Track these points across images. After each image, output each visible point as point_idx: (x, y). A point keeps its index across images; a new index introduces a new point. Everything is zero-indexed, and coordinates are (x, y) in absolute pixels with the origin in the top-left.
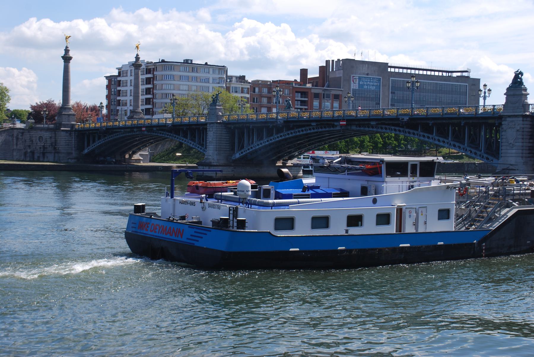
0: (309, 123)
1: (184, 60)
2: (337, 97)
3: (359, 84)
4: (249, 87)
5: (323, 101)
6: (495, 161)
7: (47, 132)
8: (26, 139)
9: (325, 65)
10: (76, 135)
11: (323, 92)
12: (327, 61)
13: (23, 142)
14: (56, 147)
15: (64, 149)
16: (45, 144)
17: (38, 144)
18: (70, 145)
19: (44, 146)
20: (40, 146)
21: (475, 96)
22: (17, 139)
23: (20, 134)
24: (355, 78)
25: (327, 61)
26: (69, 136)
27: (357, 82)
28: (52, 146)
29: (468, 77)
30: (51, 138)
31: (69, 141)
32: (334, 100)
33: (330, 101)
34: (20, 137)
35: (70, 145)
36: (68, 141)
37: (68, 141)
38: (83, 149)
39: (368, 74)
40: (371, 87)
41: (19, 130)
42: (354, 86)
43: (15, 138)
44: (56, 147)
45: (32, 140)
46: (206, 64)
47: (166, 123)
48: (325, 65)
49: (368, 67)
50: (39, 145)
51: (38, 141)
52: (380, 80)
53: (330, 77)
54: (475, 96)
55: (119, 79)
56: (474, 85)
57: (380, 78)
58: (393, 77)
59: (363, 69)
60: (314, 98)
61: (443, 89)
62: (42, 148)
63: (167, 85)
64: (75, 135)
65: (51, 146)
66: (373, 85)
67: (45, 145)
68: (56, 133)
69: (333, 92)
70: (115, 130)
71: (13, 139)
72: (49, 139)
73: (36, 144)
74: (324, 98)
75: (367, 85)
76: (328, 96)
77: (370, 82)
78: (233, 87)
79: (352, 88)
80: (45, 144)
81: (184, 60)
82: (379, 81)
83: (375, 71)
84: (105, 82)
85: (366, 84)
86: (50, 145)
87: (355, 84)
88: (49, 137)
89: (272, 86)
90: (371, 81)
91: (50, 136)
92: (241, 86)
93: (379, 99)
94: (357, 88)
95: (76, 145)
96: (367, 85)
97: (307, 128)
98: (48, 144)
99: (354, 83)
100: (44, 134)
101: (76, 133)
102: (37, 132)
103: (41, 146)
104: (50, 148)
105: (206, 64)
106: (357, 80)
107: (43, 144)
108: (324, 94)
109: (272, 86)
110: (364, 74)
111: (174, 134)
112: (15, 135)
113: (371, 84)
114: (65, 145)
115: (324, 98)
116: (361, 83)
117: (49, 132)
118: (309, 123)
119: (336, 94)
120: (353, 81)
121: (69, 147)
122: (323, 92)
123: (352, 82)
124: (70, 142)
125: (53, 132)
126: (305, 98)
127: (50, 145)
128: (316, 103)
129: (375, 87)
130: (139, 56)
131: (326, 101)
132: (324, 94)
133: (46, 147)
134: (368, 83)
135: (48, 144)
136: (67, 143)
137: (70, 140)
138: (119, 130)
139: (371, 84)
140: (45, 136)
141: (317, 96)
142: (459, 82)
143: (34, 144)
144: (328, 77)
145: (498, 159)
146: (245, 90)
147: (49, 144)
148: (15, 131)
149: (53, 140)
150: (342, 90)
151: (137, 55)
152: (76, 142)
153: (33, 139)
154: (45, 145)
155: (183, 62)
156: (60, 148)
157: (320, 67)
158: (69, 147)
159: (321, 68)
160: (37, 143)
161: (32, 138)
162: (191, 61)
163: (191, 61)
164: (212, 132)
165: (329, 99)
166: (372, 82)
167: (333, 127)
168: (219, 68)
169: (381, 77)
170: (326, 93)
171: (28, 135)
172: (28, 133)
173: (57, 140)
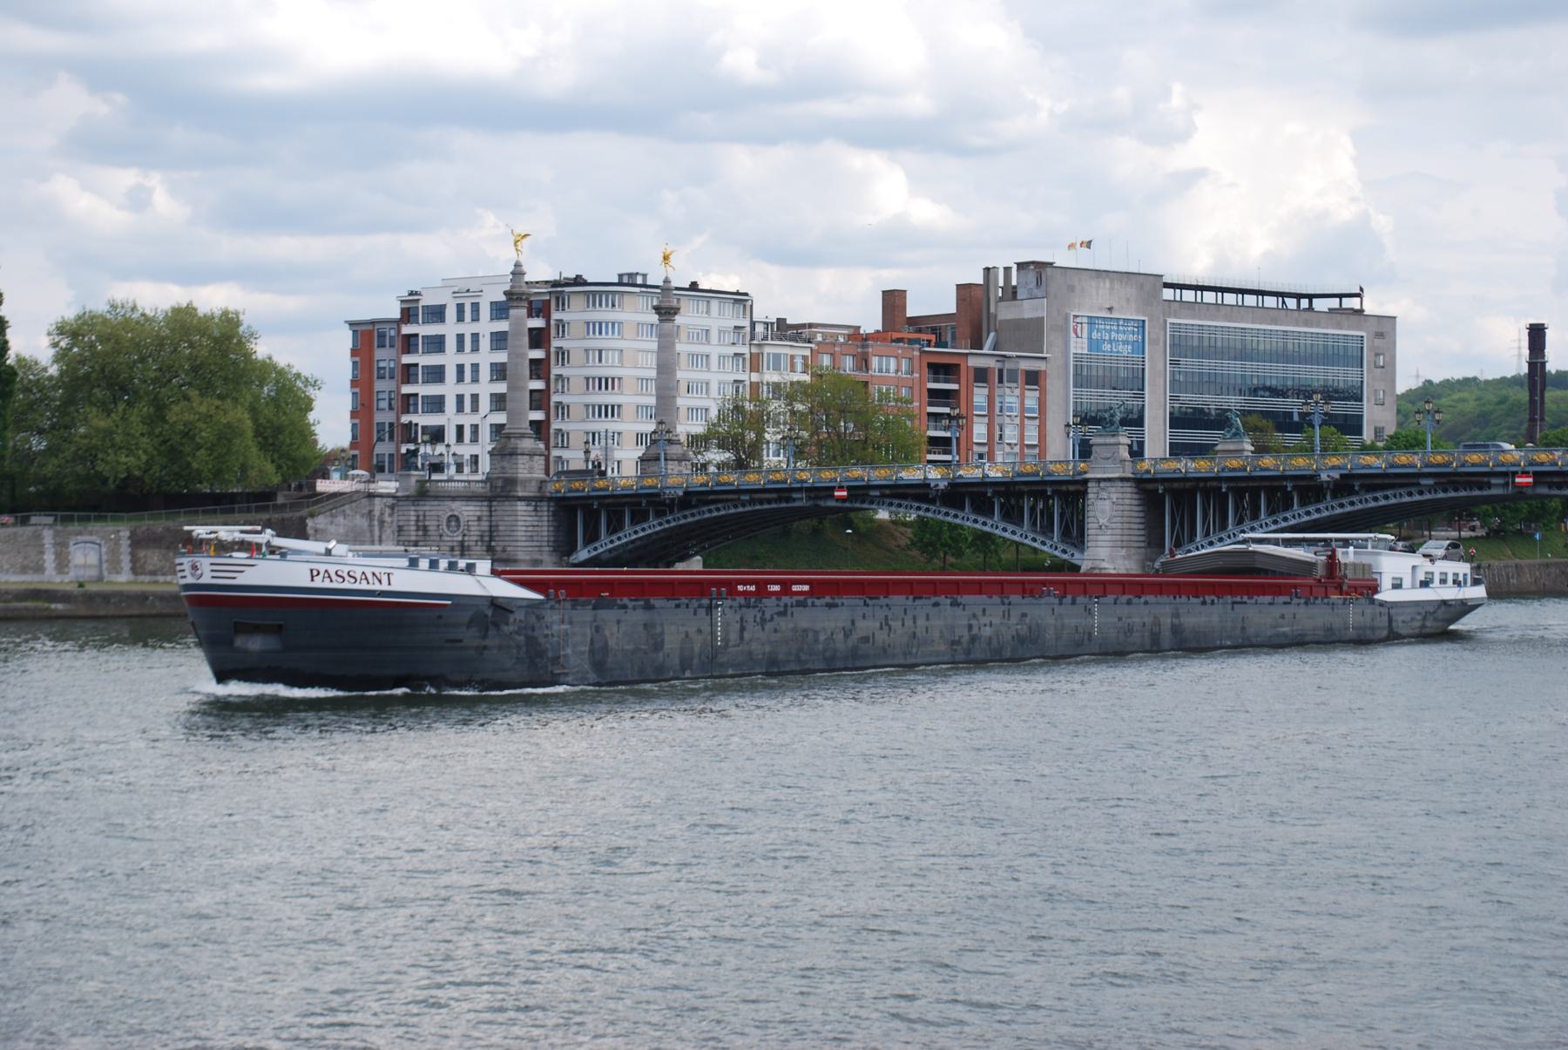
0: (1415, 481)
1: (621, 276)
2: (1033, 378)
3: (1090, 338)
4: (808, 353)
5: (998, 392)
6: (1077, 555)
7: (469, 503)
8: (401, 523)
9: (980, 281)
10: (551, 509)
11: (999, 365)
12: (987, 270)
13: (393, 532)
14: (493, 544)
15: (530, 549)
16: (464, 535)
17: (446, 538)
18: (535, 538)
19: (462, 542)
20: (450, 544)
21: (1383, 367)
22: (382, 523)
23: (388, 511)
24: (1079, 320)
25: (987, 270)
26: (533, 513)
27: (1085, 335)
28: (482, 541)
29: (1360, 312)
30: (479, 519)
31: (534, 526)
32: (1027, 387)
33: (1017, 392)
34: (388, 519)
35: (535, 538)
36: (531, 529)
37: (531, 529)
38: (572, 549)
39: (1110, 309)
40: (1121, 347)
41: (385, 500)
42: (1078, 346)
43: (376, 523)
44: (493, 544)
45: (425, 526)
46: (694, 286)
47: (926, 478)
48: (980, 281)
49: (1112, 289)
50: (449, 539)
51: (446, 529)
52: (1143, 327)
53: (1000, 317)
54: (1383, 367)
55: (407, 330)
56: (1380, 335)
57: (1144, 321)
58: (1176, 317)
59: (1098, 294)
60: (1027, 384)
61: (1183, 343)
62: (456, 548)
63: (591, 353)
64: (548, 511)
65: (479, 543)
66: (1125, 342)
67: (466, 538)
68: (491, 506)
69: (1025, 365)
70: (711, 497)
71: (371, 526)
72: (476, 523)
73: (438, 538)
74: (1001, 381)
75: (1110, 342)
76: (1013, 378)
77: (1118, 332)
78: (768, 354)
79: (1073, 350)
80: (464, 535)
81: (621, 276)
82: (1141, 329)
83: (1128, 300)
84: (346, 340)
85: (1107, 338)
86: (479, 538)
87: (1079, 340)
88: (476, 518)
89: (870, 350)
90: (1121, 328)
91: (478, 513)
92: (790, 351)
93: (1140, 382)
94: (1086, 352)
95: (552, 539)
96: (1110, 342)
97: (1367, 497)
98: (472, 538)
99: (1078, 337)
100: (463, 508)
101: (552, 504)
102: (441, 503)
103: (455, 544)
104: (479, 548)
105: (694, 286)
106: (1085, 326)
107: (460, 538)
108: (1001, 371)
109: (870, 350)
110: (1100, 309)
111: (941, 506)
112: (377, 513)
113: (1121, 337)
114: (524, 539)
115: (1001, 381)
116: (1095, 335)
117: (474, 503)
118: (1415, 481)
119: (1031, 368)
120: (1076, 333)
121: (534, 544)
122: (999, 365)
123: (1073, 335)
124: (536, 529)
125: (485, 503)
126: (947, 381)
127: (479, 538)
128: (980, 395)
129: (1130, 347)
130: (525, 268)
131: (1008, 391)
132: (1001, 371)
133: (469, 546)
134: (1114, 335)
135: (472, 538)
136: (529, 534)
137: (536, 523)
138: (735, 497)
139: (1121, 337)
140: (466, 513)
141: (981, 375)
142: (1312, 326)
143: (432, 538)
144: (992, 320)
145: (1082, 551)
146: (799, 362)
147: (475, 538)
148: (377, 500)
149: (485, 525)
150: (1045, 358)
151: (517, 265)
152: (551, 529)
153: (427, 523)
154: (466, 538)
155: (617, 281)
156: (509, 549)
157: (961, 288)
158: (534, 544)
159: (964, 290)
160: (441, 536)
161: (424, 520)
162: (645, 276)
163: (645, 276)
164: (1107, 502)
165: (1015, 385)
166: (1124, 332)
167: (1480, 488)
168: (735, 300)
169: (1146, 318)
170: (1008, 365)
171: (412, 513)
172: (413, 508)
173: (497, 526)
